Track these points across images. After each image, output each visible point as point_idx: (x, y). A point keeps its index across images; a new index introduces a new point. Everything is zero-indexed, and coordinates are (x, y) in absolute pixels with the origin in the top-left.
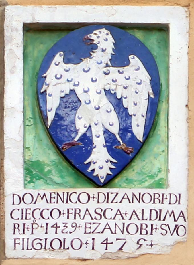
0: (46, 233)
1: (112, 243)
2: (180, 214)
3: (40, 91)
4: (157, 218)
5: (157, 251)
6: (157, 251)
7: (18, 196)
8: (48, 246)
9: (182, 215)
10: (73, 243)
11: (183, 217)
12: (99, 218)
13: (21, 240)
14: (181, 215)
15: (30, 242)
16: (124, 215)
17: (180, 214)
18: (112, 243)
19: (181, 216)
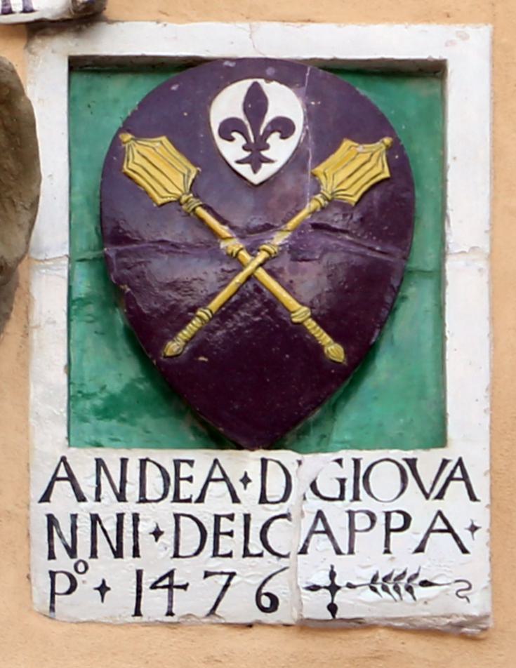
0: (420, 549)
1: (185, 587)
2: (445, 521)
3: (251, 155)
4: (165, 495)
5: (390, 656)
6: (390, 656)
7: (279, 462)
8: (256, 546)
9: (320, 527)
10: (196, 548)
11: (463, 483)
12: (368, 525)
13: (239, 520)
14: (215, 476)
15: (255, 528)
16: (238, 487)
17: (445, 521)
18: (185, 587)
19: (458, 479)
